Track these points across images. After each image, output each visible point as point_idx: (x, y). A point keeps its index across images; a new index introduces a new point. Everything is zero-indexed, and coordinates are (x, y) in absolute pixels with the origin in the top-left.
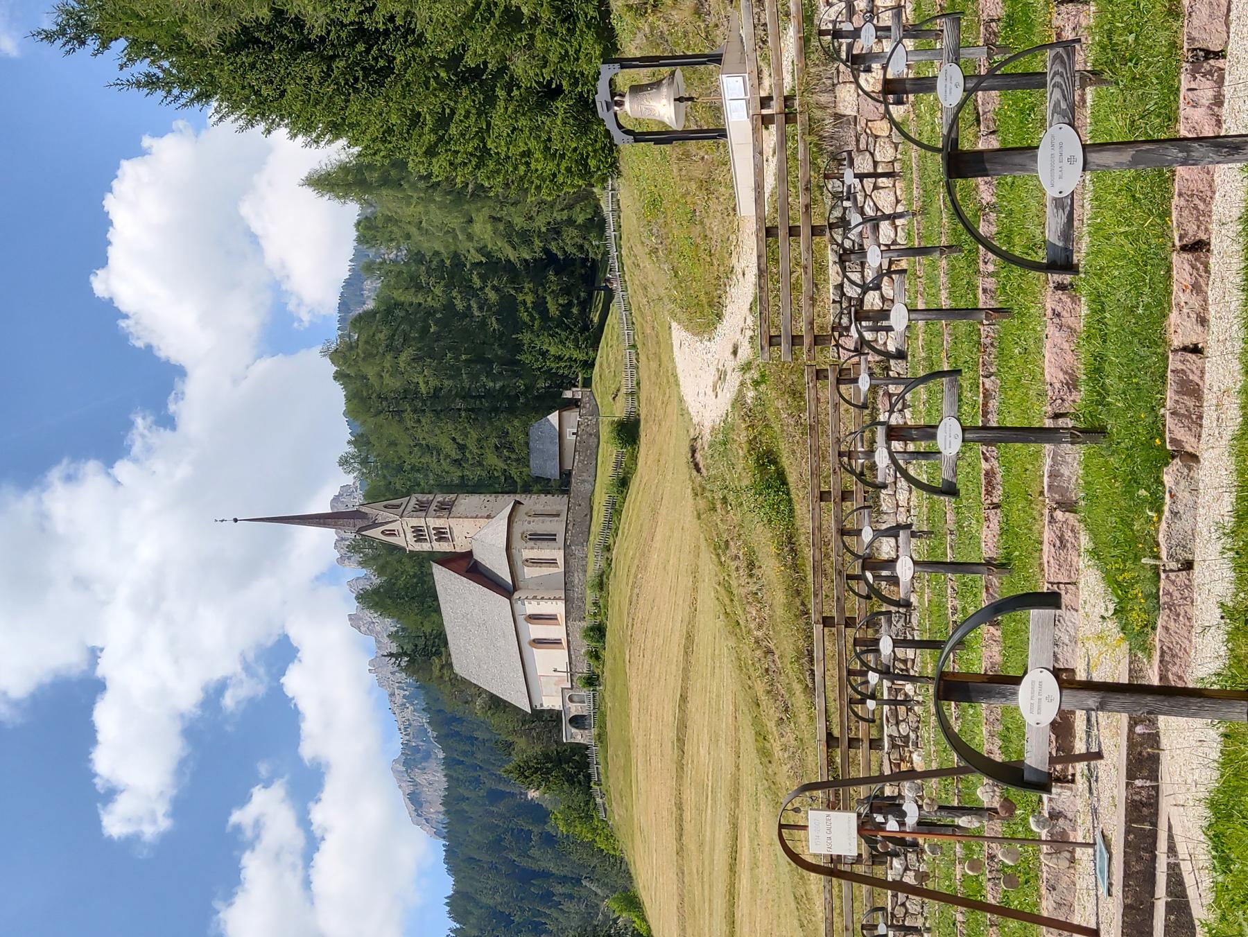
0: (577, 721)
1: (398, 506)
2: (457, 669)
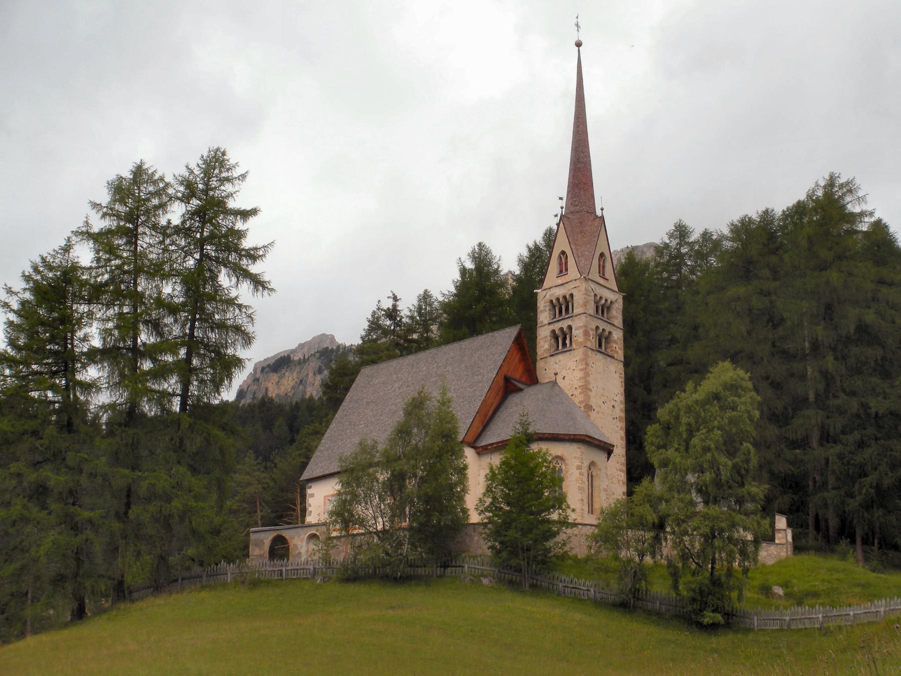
0: (280, 548)
1: (602, 274)
2: (366, 371)
